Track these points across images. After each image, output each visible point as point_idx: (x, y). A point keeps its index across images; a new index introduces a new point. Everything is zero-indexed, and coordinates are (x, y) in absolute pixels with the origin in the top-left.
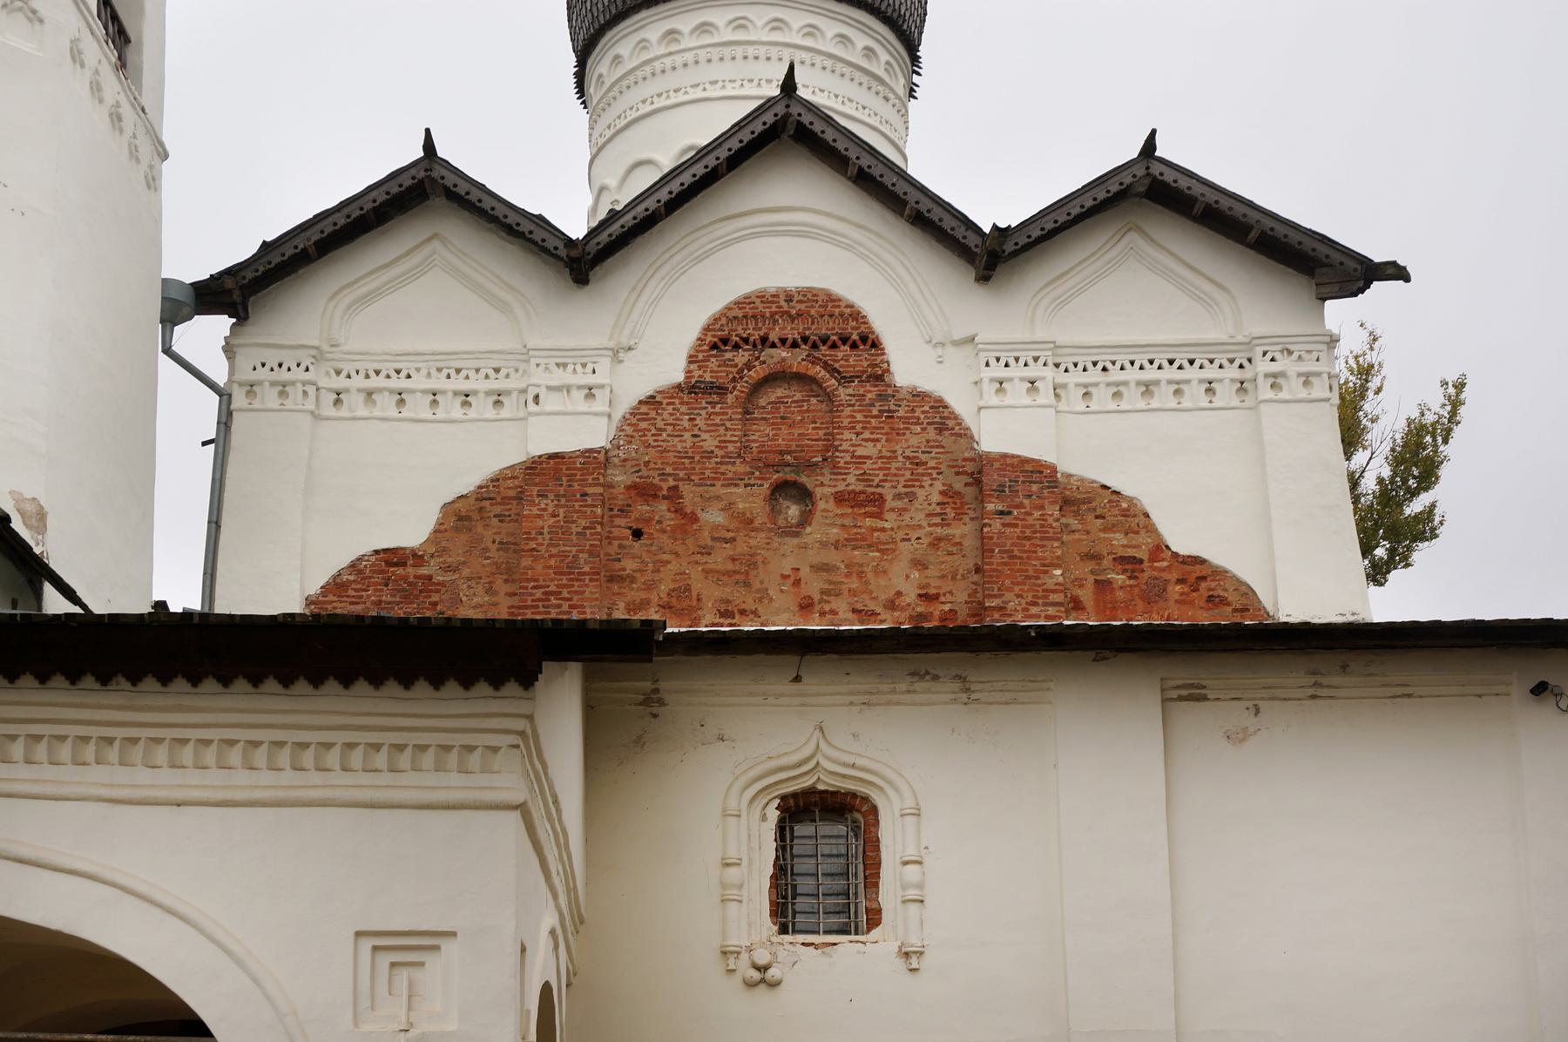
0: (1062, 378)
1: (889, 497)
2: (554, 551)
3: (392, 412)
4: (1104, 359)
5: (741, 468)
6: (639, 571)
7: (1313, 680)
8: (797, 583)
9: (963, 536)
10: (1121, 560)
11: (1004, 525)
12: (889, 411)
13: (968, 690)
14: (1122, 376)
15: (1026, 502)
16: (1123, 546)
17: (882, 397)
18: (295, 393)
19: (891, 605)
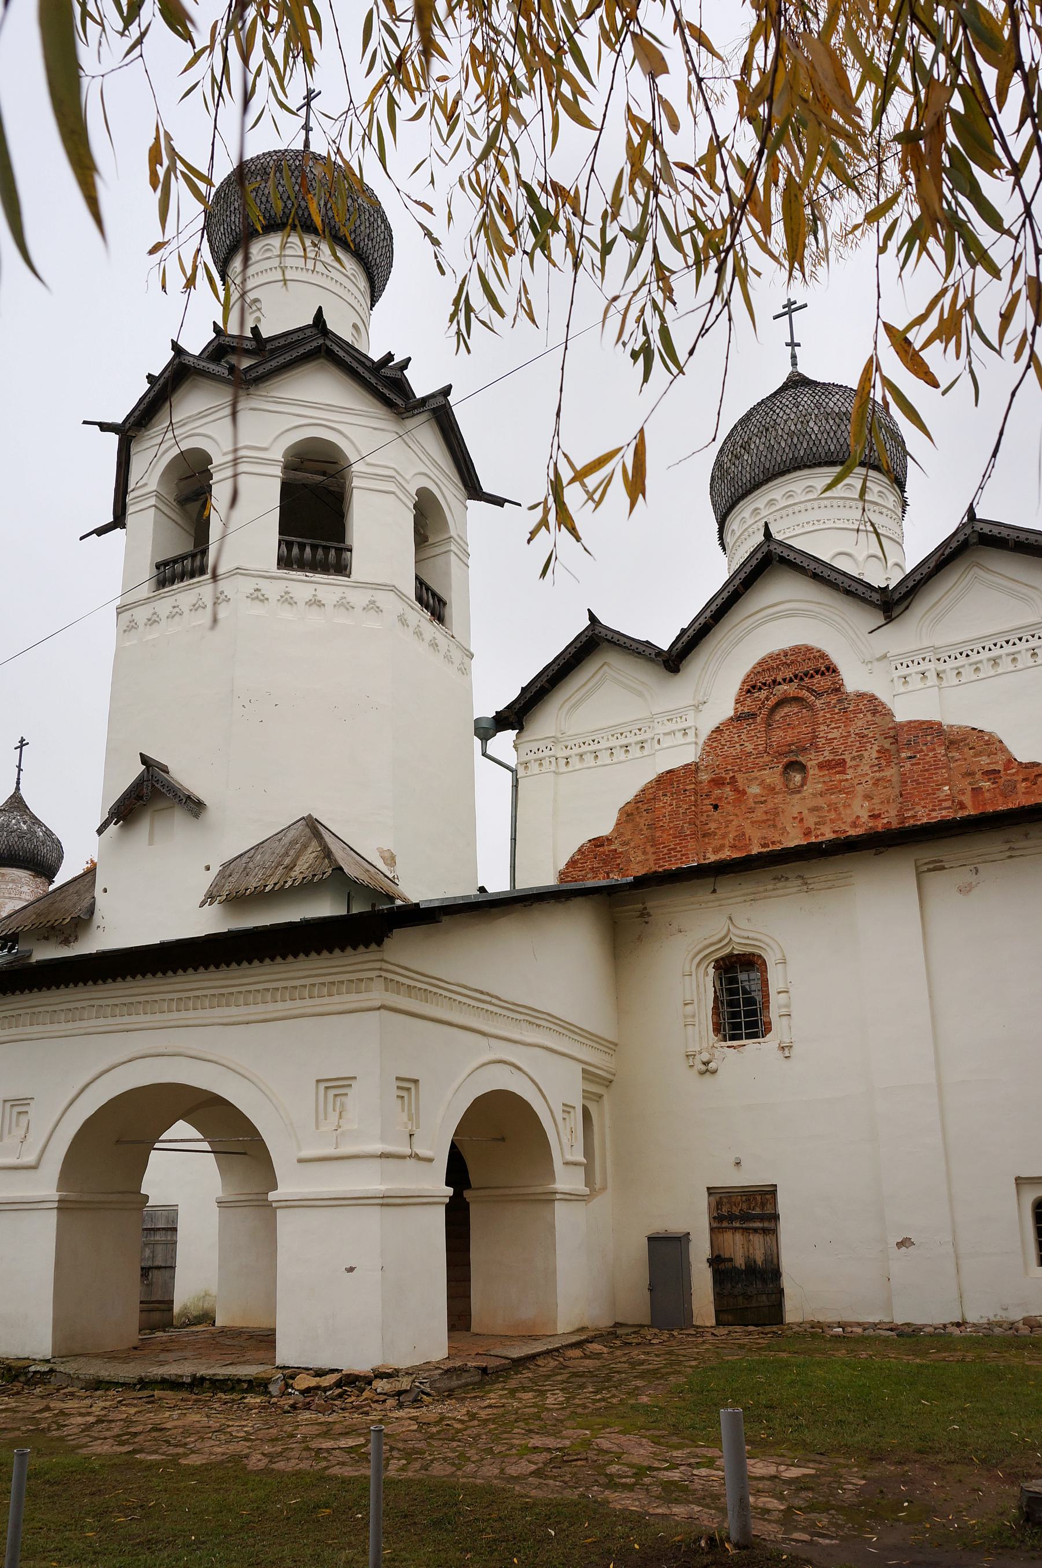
0: (941, 666)
1: (848, 760)
2: (672, 825)
3: (593, 763)
4: (966, 649)
5: (767, 758)
6: (719, 828)
7: (1008, 846)
8: (802, 820)
9: (892, 776)
10: (987, 773)
11: (912, 765)
12: (844, 708)
13: (806, 884)
14: (979, 657)
15: (924, 748)
16: (988, 764)
17: (840, 701)
18: (545, 762)
19: (854, 825)
